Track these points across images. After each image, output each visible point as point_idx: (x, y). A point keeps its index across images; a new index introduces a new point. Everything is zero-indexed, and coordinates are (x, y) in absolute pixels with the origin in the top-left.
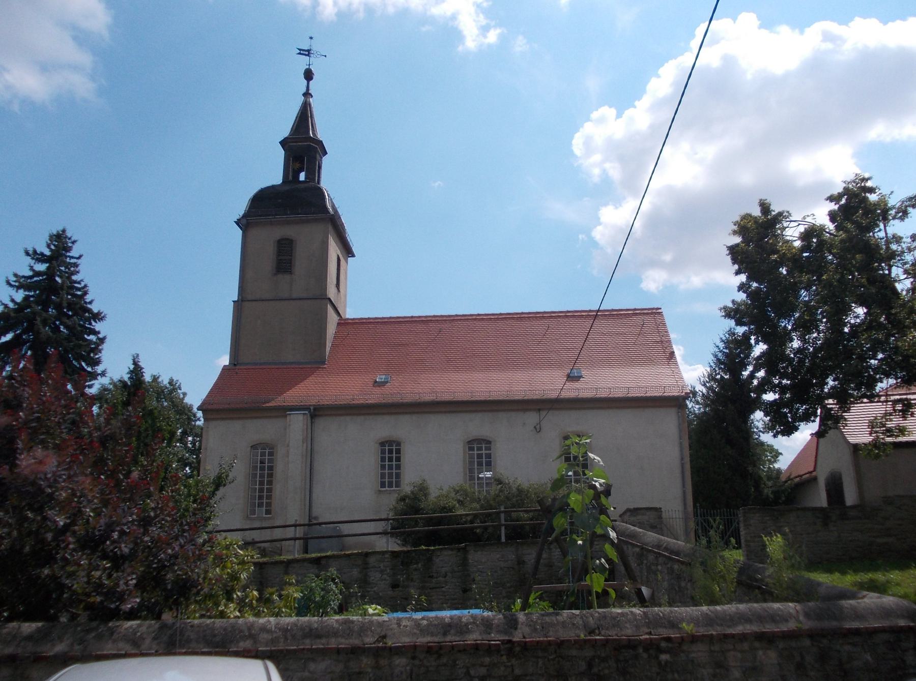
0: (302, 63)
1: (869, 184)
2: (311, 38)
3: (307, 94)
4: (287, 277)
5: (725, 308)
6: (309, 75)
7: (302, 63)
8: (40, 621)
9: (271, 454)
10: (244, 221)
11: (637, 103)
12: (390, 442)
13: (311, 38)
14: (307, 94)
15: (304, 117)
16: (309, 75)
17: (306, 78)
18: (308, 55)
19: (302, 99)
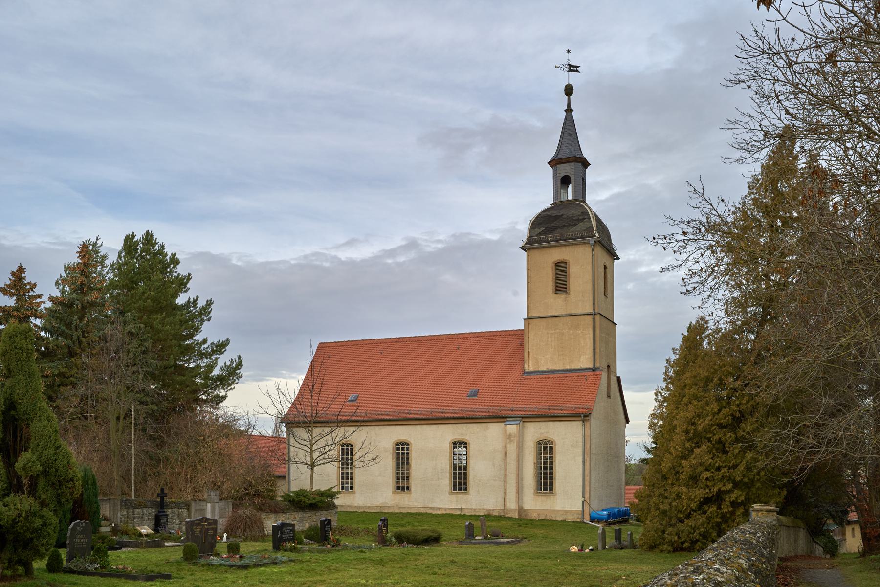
0: (564, 78)
1: (192, 300)
2: (568, 52)
3: (569, 110)
4: (563, 296)
5: (152, 235)
6: (569, 90)
7: (564, 78)
8: (663, 431)
9: (408, 449)
10: (554, 163)
11: (627, 439)
12: (403, 443)
13: (568, 52)
14: (569, 110)
15: (569, 128)
16: (569, 90)
17: (566, 94)
18: (570, 66)
19: (564, 115)
